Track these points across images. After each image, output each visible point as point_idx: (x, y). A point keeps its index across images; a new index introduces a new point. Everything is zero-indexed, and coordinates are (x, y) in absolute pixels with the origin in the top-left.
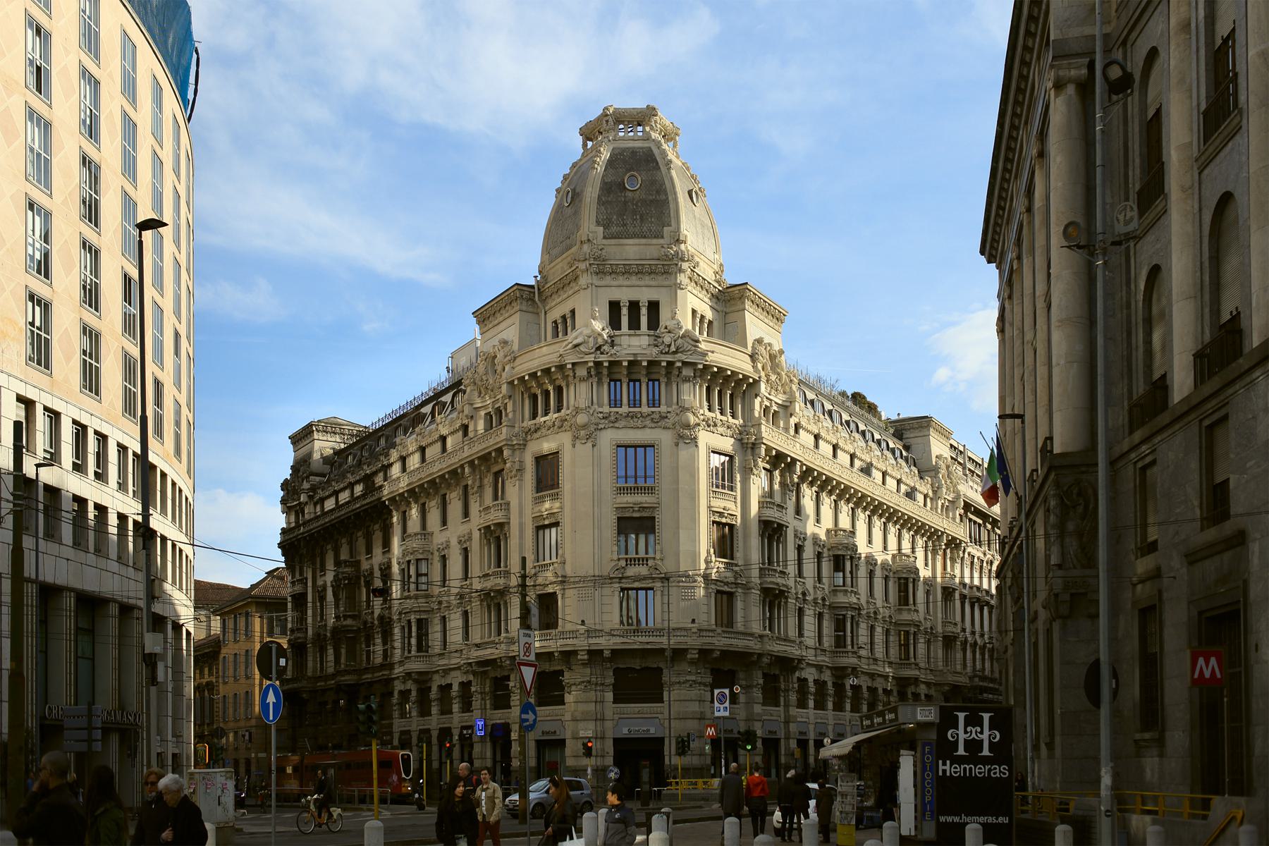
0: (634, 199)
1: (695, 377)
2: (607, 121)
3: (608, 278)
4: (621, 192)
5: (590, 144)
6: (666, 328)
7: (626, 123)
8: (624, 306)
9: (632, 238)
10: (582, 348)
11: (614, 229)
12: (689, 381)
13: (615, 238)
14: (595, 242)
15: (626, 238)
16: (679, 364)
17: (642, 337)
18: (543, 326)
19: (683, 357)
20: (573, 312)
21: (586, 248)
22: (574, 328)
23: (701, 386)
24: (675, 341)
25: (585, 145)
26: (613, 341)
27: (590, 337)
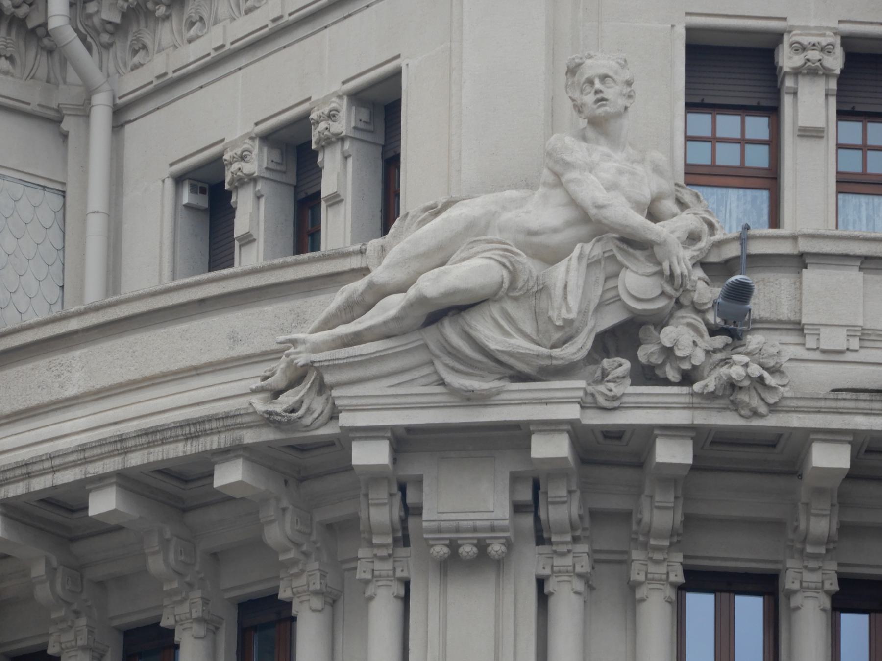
8: (813, 72)
18: (97, 197)
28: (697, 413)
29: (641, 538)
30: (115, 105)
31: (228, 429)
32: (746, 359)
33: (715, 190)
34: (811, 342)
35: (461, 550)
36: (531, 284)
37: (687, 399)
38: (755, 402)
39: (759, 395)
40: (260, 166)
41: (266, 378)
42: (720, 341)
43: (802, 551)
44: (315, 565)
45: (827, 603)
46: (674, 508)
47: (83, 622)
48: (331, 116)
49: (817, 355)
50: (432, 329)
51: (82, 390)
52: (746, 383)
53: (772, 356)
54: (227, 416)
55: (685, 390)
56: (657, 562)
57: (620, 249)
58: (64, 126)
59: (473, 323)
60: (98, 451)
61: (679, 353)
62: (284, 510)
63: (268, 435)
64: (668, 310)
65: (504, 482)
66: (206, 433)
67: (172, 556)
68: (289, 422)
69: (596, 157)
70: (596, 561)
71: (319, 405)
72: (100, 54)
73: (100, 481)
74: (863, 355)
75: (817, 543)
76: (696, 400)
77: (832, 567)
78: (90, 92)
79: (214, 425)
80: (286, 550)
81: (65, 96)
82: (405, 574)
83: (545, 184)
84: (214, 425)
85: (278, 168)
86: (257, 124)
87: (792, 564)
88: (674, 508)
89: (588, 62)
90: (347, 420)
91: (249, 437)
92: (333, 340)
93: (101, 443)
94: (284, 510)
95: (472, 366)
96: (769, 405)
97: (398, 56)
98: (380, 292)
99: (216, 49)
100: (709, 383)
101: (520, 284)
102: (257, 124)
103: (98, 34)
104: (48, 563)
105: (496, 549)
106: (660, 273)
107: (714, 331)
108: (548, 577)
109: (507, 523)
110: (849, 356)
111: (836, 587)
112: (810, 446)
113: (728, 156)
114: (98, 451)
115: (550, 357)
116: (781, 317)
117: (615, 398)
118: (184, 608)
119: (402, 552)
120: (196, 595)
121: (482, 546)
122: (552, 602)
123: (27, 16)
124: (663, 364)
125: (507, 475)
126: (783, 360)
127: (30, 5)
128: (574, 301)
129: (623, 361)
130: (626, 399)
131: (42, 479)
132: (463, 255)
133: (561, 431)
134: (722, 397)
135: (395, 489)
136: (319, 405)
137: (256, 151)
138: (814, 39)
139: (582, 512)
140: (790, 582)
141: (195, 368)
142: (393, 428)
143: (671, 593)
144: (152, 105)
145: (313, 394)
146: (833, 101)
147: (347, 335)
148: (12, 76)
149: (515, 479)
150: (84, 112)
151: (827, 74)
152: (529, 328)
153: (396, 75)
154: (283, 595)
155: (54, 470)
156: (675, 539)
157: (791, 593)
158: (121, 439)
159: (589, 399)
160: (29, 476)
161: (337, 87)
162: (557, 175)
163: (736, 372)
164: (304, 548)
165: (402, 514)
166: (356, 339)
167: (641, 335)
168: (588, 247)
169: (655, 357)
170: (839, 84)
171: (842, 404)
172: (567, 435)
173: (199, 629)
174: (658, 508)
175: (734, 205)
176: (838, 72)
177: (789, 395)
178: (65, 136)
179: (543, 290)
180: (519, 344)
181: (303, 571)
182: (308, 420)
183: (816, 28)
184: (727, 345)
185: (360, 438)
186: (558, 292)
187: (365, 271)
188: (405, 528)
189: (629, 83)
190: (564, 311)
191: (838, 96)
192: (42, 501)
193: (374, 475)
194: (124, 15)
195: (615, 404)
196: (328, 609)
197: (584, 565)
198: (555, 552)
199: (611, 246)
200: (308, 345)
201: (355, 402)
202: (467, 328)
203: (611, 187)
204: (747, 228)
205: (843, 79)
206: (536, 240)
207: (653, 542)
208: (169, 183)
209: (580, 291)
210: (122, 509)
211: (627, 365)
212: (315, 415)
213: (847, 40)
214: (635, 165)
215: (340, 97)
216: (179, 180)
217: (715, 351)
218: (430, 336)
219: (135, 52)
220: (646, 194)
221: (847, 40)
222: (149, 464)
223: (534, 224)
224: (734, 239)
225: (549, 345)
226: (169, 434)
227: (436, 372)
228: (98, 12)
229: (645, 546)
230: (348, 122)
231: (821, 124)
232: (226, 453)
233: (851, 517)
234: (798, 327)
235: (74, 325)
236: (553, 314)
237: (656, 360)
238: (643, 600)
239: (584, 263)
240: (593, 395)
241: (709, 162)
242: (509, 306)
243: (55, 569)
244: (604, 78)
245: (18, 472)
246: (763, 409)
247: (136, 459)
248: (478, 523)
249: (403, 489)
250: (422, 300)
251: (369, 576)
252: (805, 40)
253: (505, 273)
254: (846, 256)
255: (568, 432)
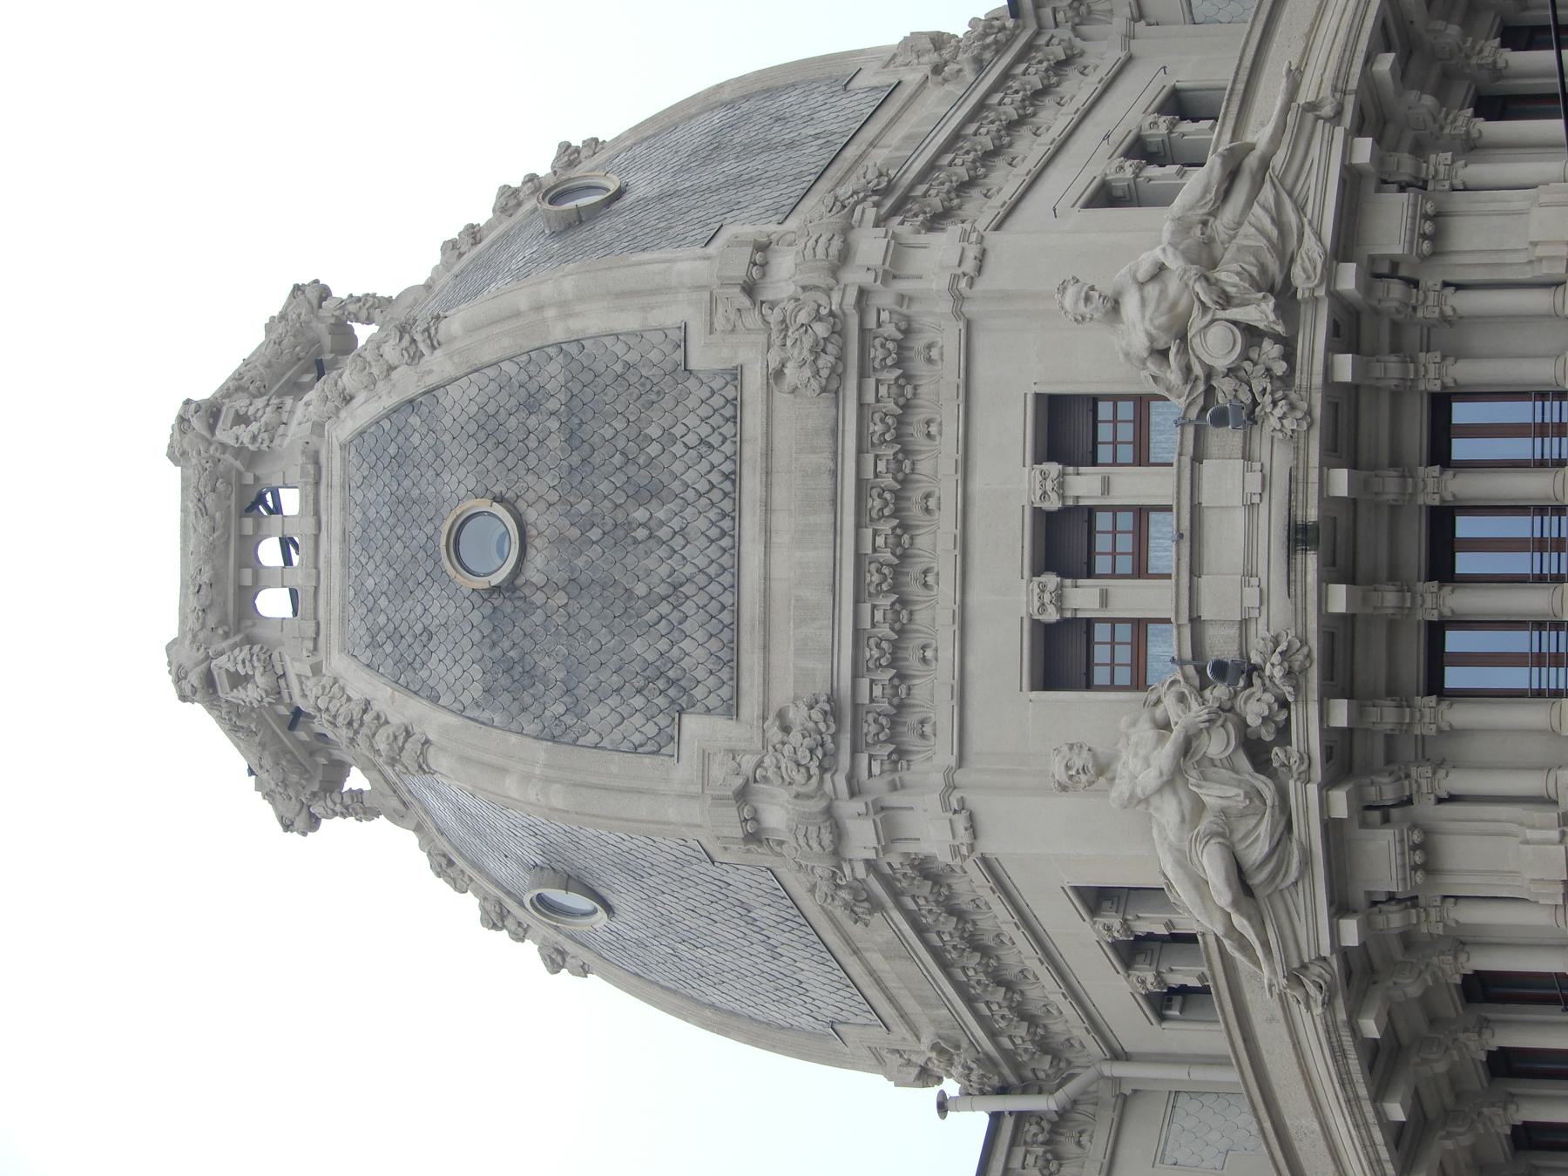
0: (561, 539)
1: (1418, 184)
2: (237, 680)
3: (921, 689)
4: (529, 608)
5: (356, 780)
6: (1164, 353)
7: (247, 580)
8: (1059, 598)
9: (736, 550)
10: (1256, 851)
11: (695, 652)
12: (1438, 217)
13: (735, 646)
14: (748, 762)
15: (735, 587)
16: (1348, 278)
17: (1206, 498)
18: (1178, 1073)
19: (1312, 251)
20: (1096, 899)
21: (776, 815)
22: (1153, 895)
23: (1472, 148)
24: (1226, 301)
25: (359, 807)
26: (1221, 669)
27: (1199, 806)
28: (1309, 697)
29: (1405, 728)
30: (1111, 1059)
31: (1336, 1029)
32: (1268, 665)
33: (1149, 664)
34: (1255, 613)
35: (1427, 231)
36: (1220, 821)
37: (1300, 705)
38: (1300, 657)
39: (1294, 654)
40: (1149, 971)
41: (1298, 1002)
42: (1256, 681)
43: (1411, 494)
44: (1435, 960)
45: (1447, 589)
46: (1383, 477)
47: (1486, 1110)
48: (1109, 929)
49: (1264, 609)
50: (1257, 892)
51: (1315, 1119)
52: (1286, 665)
53: (1266, 645)
54: (1327, 1031)
55: (1293, 707)
56: (1422, 716)
57: (1192, 757)
58: (1128, 1093)
59: (1250, 863)
60: (1358, 1117)
61: (1266, 713)
62: (1395, 983)
63: (1340, 1003)
64: (1236, 718)
65: (1365, 832)
66: (1341, 1045)
67: (1434, 1057)
68: (1329, 990)
69: (1125, 773)
70: (1423, 757)
71: (1316, 970)
72: (1075, 1067)
73: (1380, 1115)
74: (1263, 575)
75: (1404, 486)
76: (1300, 698)
77: (1420, 586)
78: (1102, 1077)
79: (1334, 1039)
80: (1425, 980)
81: (1107, 1094)
82: (1439, 899)
83: (1147, 809)
84: (1334, 1039)
85: (1149, 956)
86: (1118, 973)
87: (1422, 386)
88: (1383, 477)
89: (1057, 777)
90: (1325, 951)
91: (1342, 1016)
92: (1268, 960)
93: (1352, 1114)
94: (1395, 983)
95: (1283, 861)
96: (1301, 646)
97: (1063, 888)
98: (1231, 929)
99: (1066, 998)
100: (1287, 690)
101: (1220, 830)
102: (1118, 973)
103: (1060, 1069)
104: (1443, 1138)
105: (1416, 837)
106: (1208, 729)
107: (1250, 684)
108: (1436, 795)
109: (1396, 832)
110: (1264, 585)
111: (1437, 468)
112: (1338, 292)
113: (1126, 432)
114: (1358, 1117)
115: (1273, 807)
116: (1237, 635)
117: (1301, 758)
118: (1472, 1045)
119: (1422, 901)
120: (1462, 1036)
121: (1415, 847)
122: (1454, 792)
123: (1049, 1121)
124: (1275, 723)
125: (1363, 831)
126: (1268, 635)
127: (1042, 1119)
128: (1232, 792)
129: (1274, 752)
130: (1302, 750)
131: (1380, 1152)
132: (1201, 869)
133: (1327, 796)
134: (1297, 680)
135: (1376, 909)
136: (1316, 970)
137: (1138, 973)
138: (1036, 598)
139: (1387, 774)
140: (1436, 387)
141: (1294, 1045)
142: (1331, 917)
143: (1450, 473)
144: (1109, 1035)
145: (1307, 973)
146: (1081, 582)
147: (1264, 951)
148: (1093, 1132)
149: (1364, 824)
150: (1117, 1081)
151: (1061, 587)
152: (1253, 822)
153: (1077, 889)
154: (1458, 980)
155: (1373, 1144)
156: (1404, 703)
157: (1444, 386)
158: (1348, 1101)
159: (1303, 776)
160: (1379, 1161)
161: (1087, 925)
162: (1140, 801)
163: (1278, 673)
164: (1422, 967)
165: (1394, 903)
166: (1265, 944)
167: (1254, 738)
168: (1192, 780)
169: (1269, 729)
170: (1070, 465)
171: (1299, 592)
172: (1330, 792)
173: (1487, 1034)
174: (1381, 719)
175: (1160, 650)
176: (1061, 467)
177: (1294, 632)
178: (1135, 1091)
179: (1224, 812)
180: (1264, 828)
181: (1440, 968)
182: (1328, 977)
183: (1027, 596)
184: (1259, 676)
185: (1339, 940)
186: (1225, 803)
187: (1217, 939)
188: (1405, 900)
189: (1071, 747)
190: (1238, 799)
191: (1077, 465)
192: (1397, 1148)
193: (1366, 927)
194: (1046, 1052)
195: (1306, 757)
196: (1467, 948)
197: (1427, 771)
198: (1417, 792)
199: (1190, 763)
200: (1272, 977)
201: (1312, 946)
202: (1254, 867)
203: (1147, 763)
204: (1173, 660)
205: (1063, 574)
206: (1187, 817)
207: (1407, 721)
208: (1165, 1025)
209: (1223, 787)
210: (1399, 1098)
211: (1276, 749)
212: (1323, 972)
213: (1036, 573)
214: (1131, 743)
215: (1095, 923)
216: (1162, 1018)
217: (1264, 685)
218: (1261, 893)
219: (1072, 1045)
220: (1150, 734)
221: (1037, 460)
222: (1365, 1082)
223: (1175, 818)
224: (1182, 669)
225: (1264, 807)
226: (1342, 1070)
227: (1288, 888)
228: (1044, 1071)
229: (1413, 495)
230: (1112, 917)
231: (1097, 591)
232: (1355, 1031)
233: (1384, 574)
234: (1244, 623)
235: (1268, 1125)
236: (1241, 806)
237: (1272, 727)
238: (1451, 726)
239: (1203, 783)
240: (1300, 773)
241: (1132, 425)
242: (1237, 836)
243: (1448, 1132)
244: (1068, 768)
245: (1376, 1168)
246: (1305, 650)
247: (1363, 1091)
248: (1398, 851)
249: (1375, 903)
250: (1235, 904)
251: (1441, 924)
252: (1037, 605)
253: (1212, 841)
254: (1190, 588)
255: (1328, 790)
